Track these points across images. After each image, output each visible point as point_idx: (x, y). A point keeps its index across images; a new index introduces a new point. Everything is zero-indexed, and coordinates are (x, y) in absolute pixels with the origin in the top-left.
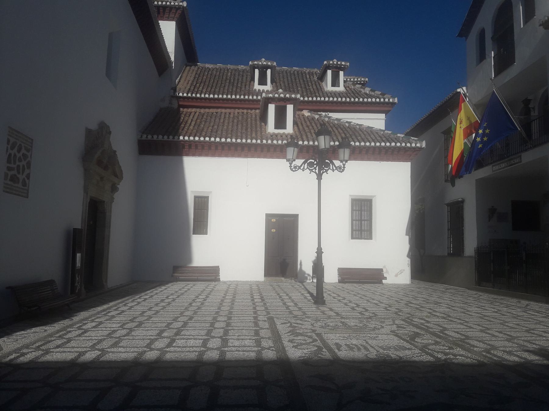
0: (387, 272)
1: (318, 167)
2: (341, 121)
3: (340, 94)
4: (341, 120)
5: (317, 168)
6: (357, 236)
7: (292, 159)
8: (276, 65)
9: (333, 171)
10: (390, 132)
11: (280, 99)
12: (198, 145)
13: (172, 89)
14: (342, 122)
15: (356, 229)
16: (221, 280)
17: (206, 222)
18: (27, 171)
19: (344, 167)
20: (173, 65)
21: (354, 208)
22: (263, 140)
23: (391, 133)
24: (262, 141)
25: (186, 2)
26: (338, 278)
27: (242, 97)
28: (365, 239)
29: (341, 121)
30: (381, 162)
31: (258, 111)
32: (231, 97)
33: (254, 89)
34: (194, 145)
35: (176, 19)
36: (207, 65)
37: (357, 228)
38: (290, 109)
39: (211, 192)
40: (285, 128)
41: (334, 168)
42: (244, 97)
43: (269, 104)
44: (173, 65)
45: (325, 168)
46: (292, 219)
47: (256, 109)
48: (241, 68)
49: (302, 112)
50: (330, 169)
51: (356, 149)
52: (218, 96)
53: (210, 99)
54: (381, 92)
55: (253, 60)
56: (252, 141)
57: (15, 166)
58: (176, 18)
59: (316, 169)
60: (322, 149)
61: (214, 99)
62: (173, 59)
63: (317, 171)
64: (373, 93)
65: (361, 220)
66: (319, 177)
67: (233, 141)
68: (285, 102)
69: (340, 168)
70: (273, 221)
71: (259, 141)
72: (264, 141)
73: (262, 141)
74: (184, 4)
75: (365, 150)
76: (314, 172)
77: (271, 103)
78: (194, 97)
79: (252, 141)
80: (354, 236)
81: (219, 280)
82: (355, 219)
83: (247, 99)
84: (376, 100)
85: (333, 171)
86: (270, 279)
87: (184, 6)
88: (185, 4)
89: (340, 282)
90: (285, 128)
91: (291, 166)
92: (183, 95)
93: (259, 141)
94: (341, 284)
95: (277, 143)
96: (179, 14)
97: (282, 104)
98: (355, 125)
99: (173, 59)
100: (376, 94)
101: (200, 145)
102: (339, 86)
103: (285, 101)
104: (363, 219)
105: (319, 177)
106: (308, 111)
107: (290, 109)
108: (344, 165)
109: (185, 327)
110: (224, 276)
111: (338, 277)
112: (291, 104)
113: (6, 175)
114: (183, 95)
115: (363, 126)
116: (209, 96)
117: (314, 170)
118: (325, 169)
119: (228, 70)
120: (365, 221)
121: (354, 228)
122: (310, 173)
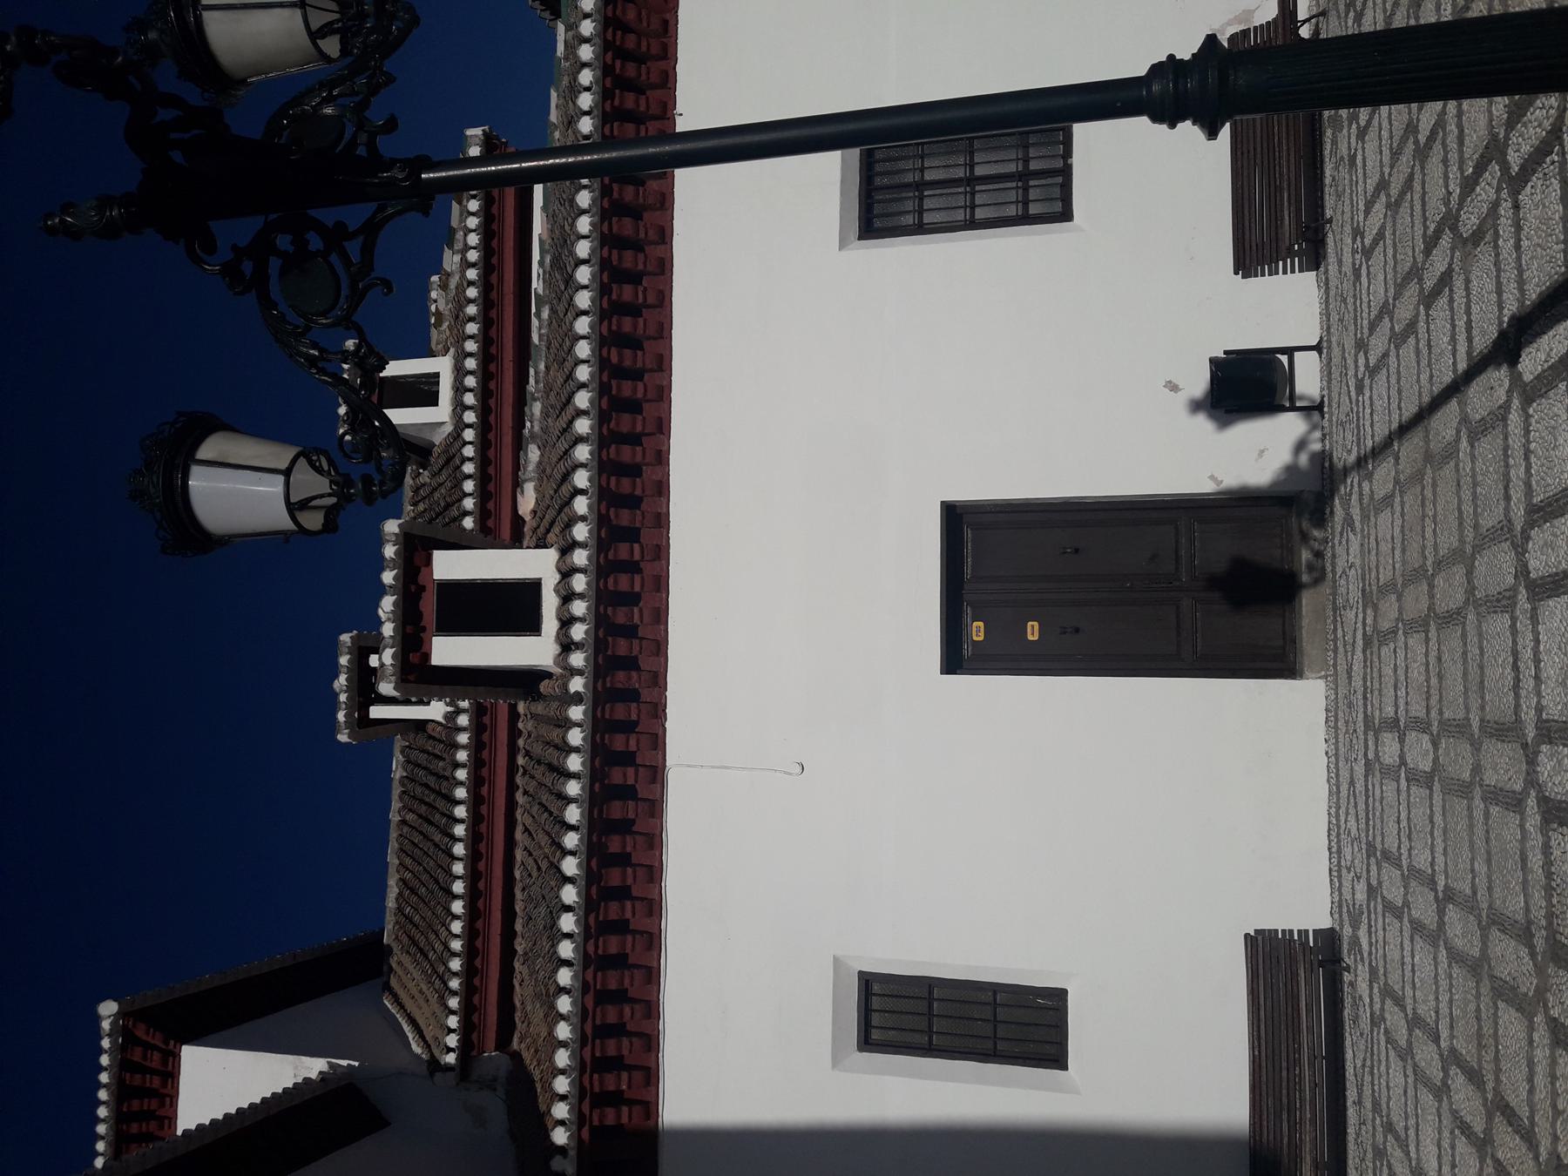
0: (1249, 13)
1: (313, 213)
5: (328, 216)
6: (1057, 192)
7: (287, 473)
8: (350, 635)
10: (554, 95)
11: (409, 615)
12: (598, 1022)
13: (432, 1074)
15: (1017, 202)
16: (1326, 923)
17: (995, 993)
20: (344, 1063)
21: (909, 220)
22: (567, 690)
23: (557, 91)
24: (577, 699)
25: (101, 1005)
26: (1293, 271)
27: (461, 774)
28: (1068, 153)
30: (679, 109)
31: (521, 707)
32: (461, 821)
33: (444, 722)
34: (598, 1041)
35: (172, 1043)
36: (391, 903)
37: (1012, 196)
38: (450, 565)
39: (836, 960)
40: (534, 586)
42: (463, 766)
44: (344, 1063)
47: (514, 716)
48: (400, 769)
49: (528, 518)
51: (615, 229)
52: (459, 878)
53: (474, 915)
54: (454, 202)
55: (333, 727)
56: (577, 750)
58: (167, 1044)
59: (341, 225)
61: (473, 897)
62: (314, 1067)
63: (355, 215)
64: (457, 236)
65: (971, 181)
67: (576, 842)
68: (423, 588)
70: (982, 634)
71: (576, 713)
72: (577, 685)
73: (577, 699)
74: (110, 1014)
75: (615, 187)
76: (368, 250)
77: (427, 656)
78: (460, 984)
79: (577, 750)
80: (1058, 207)
81: (1329, 938)
82: (962, 211)
83: (468, 756)
84: (473, 214)
86: (1310, 644)
87: (118, 1013)
88: (108, 1008)
89: (1314, 258)
90: (534, 586)
92: (453, 1031)
93: (576, 713)
94: (1339, 243)
95: (582, 620)
96: (152, 1030)
97: (429, 606)
99: (314, 1067)
101: (598, 1010)
102: (437, 375)
103: (413, 588)
104: (962, 175)
106: (518, 495)
107: (450, 565)
111: (1285, 272)
112: (429, 562)
114: (453, 1031)
116: (456, 917)
117: (354, 248)
119: (404, 822)
120: (977, 203)
121: (1011, 211)
122: (387, 284)
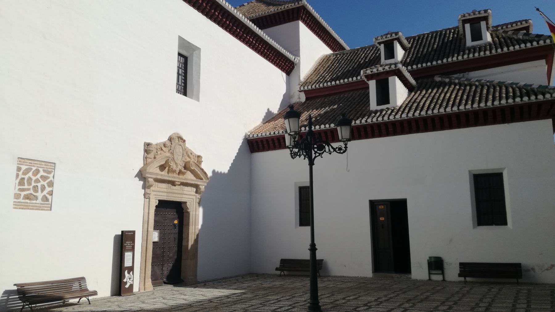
2: (472, 80)
3: (490, 46)
4: (471, 79)
9: (330, 154)
14: (472, 82)
18: (48, 189)
19: (346, 148)
29: (472, 80)
41: (332, 150)
43: (545, 60)
45: (318, 152)
46: (132, 233)
50: (325, 151)
57: (31, 187)
60: (339, 126)
66: (311, 163)
69: (340, 149)
70: (381, 208)
85: (330, 154)
91: (291, 154)
98: (485, 83)
100: (531, 37)
105: (311, 163)
108: (346, 145)
109: (460, 301)
110: (428, 259)
113: (17, 196)
115: (493, 83)
118: (318, 153)
